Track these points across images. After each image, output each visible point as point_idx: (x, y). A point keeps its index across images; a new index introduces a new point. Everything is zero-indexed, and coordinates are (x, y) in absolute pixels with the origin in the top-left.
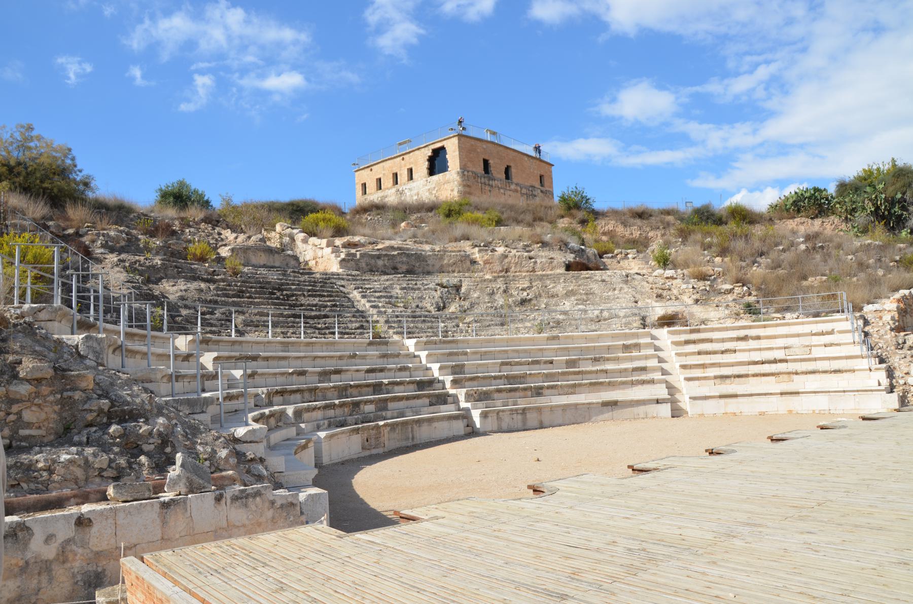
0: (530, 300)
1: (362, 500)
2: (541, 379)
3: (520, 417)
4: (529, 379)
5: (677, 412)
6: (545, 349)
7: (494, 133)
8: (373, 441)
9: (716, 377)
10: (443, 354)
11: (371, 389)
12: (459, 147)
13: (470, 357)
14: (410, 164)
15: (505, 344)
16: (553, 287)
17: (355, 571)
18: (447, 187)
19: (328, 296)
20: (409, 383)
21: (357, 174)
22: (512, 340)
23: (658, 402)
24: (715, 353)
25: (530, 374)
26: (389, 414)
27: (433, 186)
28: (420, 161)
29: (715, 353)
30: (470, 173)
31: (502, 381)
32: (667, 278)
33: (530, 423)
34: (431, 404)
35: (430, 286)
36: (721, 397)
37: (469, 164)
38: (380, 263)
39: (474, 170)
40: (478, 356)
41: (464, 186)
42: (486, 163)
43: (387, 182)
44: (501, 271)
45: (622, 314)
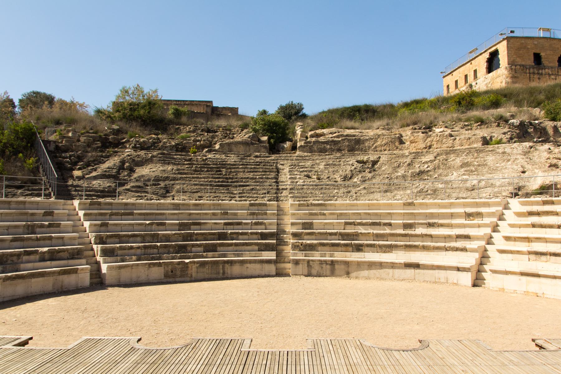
0: (428, 171)
1: (24, 303)
2: (372, 238)
3: (328, 267)
4: (361, 237)
5: (477, 282)
6: (393, 213)
7: (545, 30)
8: (178, 273)
9: (530, 253)
10: (305, 214)
12: (508, 47)
13: (269, 217)
14: (476, 66)
15: (35, 206)
16: (453, 160)
17: (302, 363)
18: (500, 79)
19: (262, 172)
22: (373, 205)
23: (458, 269)
24: (551, 227)
25: (361, 233)
27: (489, 81)
28: (481, 63)
29: (551, 227)
30: (518, 67)
31: (337, 237)
33: (314, 272)
34: (260, 250)
36: (523, 274)
39: (523, 63)
40: (336, 216)
41: (512, 77)
42: (537, 58)
43: (461, 83)
44: (426, 148)
45: (498, 184)
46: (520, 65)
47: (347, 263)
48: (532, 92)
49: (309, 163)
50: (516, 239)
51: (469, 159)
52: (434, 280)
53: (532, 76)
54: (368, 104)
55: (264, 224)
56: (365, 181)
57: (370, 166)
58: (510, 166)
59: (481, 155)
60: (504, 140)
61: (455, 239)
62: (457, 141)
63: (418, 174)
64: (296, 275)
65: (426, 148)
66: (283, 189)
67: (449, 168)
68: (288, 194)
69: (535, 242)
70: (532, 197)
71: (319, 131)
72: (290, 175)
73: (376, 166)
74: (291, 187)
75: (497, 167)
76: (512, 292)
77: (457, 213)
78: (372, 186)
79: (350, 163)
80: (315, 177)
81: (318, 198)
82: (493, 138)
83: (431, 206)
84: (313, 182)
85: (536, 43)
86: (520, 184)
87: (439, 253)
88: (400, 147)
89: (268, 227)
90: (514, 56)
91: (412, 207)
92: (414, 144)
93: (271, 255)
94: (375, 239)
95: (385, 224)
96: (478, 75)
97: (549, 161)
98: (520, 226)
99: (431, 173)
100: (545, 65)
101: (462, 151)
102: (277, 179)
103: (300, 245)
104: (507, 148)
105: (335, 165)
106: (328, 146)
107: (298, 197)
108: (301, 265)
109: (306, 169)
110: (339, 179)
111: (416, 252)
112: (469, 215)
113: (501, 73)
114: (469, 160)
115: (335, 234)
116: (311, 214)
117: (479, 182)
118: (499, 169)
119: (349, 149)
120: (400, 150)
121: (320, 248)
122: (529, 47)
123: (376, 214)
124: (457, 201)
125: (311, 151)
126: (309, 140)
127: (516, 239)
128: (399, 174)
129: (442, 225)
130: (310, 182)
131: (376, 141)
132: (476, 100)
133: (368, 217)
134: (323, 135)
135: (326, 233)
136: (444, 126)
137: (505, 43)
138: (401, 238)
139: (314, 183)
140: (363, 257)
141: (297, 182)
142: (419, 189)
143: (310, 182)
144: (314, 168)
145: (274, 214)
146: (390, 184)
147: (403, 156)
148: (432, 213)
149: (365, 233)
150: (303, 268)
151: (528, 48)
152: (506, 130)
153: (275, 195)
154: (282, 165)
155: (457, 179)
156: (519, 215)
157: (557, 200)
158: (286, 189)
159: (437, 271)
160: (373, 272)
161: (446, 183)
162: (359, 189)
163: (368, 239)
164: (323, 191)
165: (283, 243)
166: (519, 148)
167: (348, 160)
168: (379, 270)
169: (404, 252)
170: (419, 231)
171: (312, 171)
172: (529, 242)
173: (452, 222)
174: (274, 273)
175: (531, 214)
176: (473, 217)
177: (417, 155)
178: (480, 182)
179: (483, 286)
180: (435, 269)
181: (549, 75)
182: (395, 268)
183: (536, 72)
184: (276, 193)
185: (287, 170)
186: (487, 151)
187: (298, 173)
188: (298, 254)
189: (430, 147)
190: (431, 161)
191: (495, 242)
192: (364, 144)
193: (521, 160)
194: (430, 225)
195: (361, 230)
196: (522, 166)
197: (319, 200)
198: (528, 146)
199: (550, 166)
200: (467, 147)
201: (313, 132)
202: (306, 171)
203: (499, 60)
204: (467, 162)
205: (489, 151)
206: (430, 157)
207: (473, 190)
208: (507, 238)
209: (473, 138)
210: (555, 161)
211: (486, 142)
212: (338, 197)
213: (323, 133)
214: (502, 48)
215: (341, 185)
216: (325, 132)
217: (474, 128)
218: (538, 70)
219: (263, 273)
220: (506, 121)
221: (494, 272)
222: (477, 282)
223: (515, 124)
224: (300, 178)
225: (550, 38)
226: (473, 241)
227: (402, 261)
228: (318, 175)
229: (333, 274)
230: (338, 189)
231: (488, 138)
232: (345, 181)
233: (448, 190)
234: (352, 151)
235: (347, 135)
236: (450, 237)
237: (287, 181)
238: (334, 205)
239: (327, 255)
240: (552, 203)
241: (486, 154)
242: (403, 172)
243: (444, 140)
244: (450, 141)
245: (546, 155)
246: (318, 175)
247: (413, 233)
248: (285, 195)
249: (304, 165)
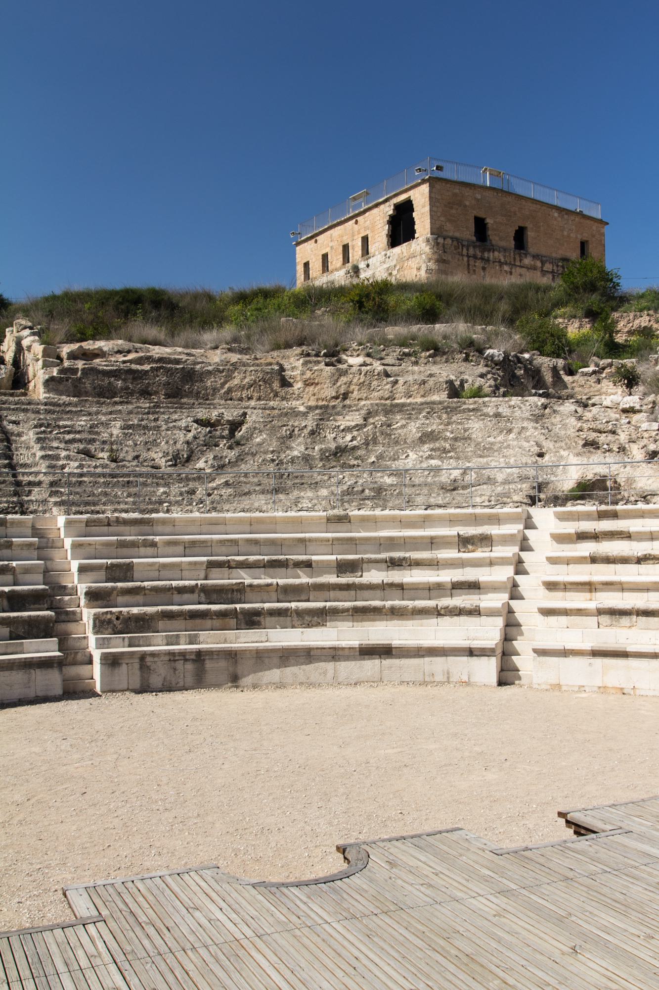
0: (354, 448)
2: (274, 596)
3: (189, 666)
4: (249, 595)
5: (507, 676)
6: (310, 540)
9: (600, 612)
10: (108, 544)
12: (430, 197)
13: (16, 552)
14: (366, 228)
15: (248, 528)
16: (403, 426)
18: (414, 262)
21: (298, 248)
22: (260, 521)
23: (471, 652)
24: (624, 560)
25: (251, 586)
27: (394, 262)
29: (624, 560)
30: (449, 241)
31: (195, 597)
32: (625, 411)
33: (155, 681)
35: (179, 424)
36: (596, 653)
37: (448, 226)
39: (457, 235)
40: (180, 549)
42: (480, 226)
43: (336, 260)
44: (336, 398)
45: (500, 477)
46: (452, 238)
47: (232, 656)
48: (488, 294)
49: (82, 422)
50: (566, 587)
51: (434, 425)
52: (421, 678)
53: (472, 263)
54: (157, 288)
55: (12, 570)
56: (222, 467)
57: (226, 432)
58: (515, 443)
59: (454, 418)
60: (487, 390)
61: (449, 592)
62: (400, 387)
63: (335, 454)
64: (113, 691)
65: (336, 398)
66: (30, 483)
67: (397, 443)
68: (45, 495)
69: (602, 590)
70: (569, 504)
71: (89, 345)
72: (42, 448)
73: (238, 435)
74: (51, 478)
75: (492, 444)
76: (576, 689)
77: (443, 537)
78: (242, 479)
79: (181, 426)
80: (105, 455)
81: (122, 506)
82: (466, 385)
83: (382, 523)
84: (104, 466)
85: (479, 196)
86: (540, 480)
87: (425, 621)
88: (282, 393)
89: (20, 577)
90: (442, 219)
91: (346, 526)
92: (311, 388)
93: (45, 648)
94: (281, 597)
95: (298, 564)
96: (371, 249)
97: (583, 435)
98: (569, 561)
99: (360, 453)
100: (494, 242)
101: (419, 408)
102: (10, 458)
103: (114, 618)
104: (493, 404)
105: (145, 427)
106: (120, 383)
107: (73, 504)
108: (124, 667)
109: (78, 436)
110: (162, 462)
111: (378, 623)
112: (465, 542)
113: (418, 249)
114: (434, 427)
115: (191, 590)
116: (122, 545)
117: (464, 473)
118: (495, 448)
119: (169, 391)
120: (283, 399)
121: (161, 624)
122: (467, 203)
123: (272, 542)
124: (429, 512)
125: (77, 392)
126: (66, 364)
127: (566, 587)
128: (296, 453)
129: (418, 564)
130: (96, 467)
131: (229, 377)
132: (391, 300)
133: (254, 549)
134: (99, 354)
135: (170, 589)
136: (364, 352)
137: (425, 188)
138: (339, 594)
139: (107, 471)
140: (264, 639)
141: (63, 467)
142: (345, 487)
143: (96, 467)
144: (98, 433)
145: (30, 545)
146: (282, 476)
147: (295, 413)
148: (391, 539)
149: (259, 586)
150: (128, 673)
151: (465, 206)
152: (482, 369)
153: (15, 499)
154: (14, 422)
155: (418, 466)
156: (560, 539)
157: (624, 510)
158: (39, 483)
159: (427, 660)
160: (290, 671)
161: (397, 473)
162: (213, 485)
163: (265, 598)
164: (133, 490)
165: (63, 617)
166: (524, 408)
167: (176, 417)
168: (304, 667)
169: (351, 624)
170: (374, 576)
171: (94, 440)
172: (591, 591)
173: (439, 556)
174: (59, 691)
175: (582, 537)
176: (473, 544)
177: (326, 412)
178: (465, 472)
179: (517, 682)
180: (423, 656)
181: (501, 264)
182: (339, 660)
183: (479, 254)
184: (16, 494)
185: (30, 436)
186: (464, 411)
187: (62, 445)
188: (113, 642)
189: (345, 396)
190: (359, 427)
191: (524, 594)
192: (202, 381)
193: (533, 432)
194: (395, 564)
195: (246, 578)
196: (538, 445)
197: (126, 511)
198: (540, 404)
199: (584, 445)
200: (419, 400)
201: (74, 346)
202: (80, 441)
203: (413, 223)
204: (433, 432)
205: (470, 410)
206: (353, 419)
207: (454, 490)
208: (551, 586)
209: (431, 382)
210: (592, 436)
211: (455, 391)
212: (170, 502)
213: (100, 349)
214: (420, 197)
215: (170, 475)
216: (105, 349)
217: (422, 360)
218: (483, 252)
219: (32, 694)
220: (481, 351)
221: (541, 653)
222: (507, 676)
223: (496, 358)
224: (68, 458)
225: (502, 191)
226: (486, 593)
227: (355, 643)
228: (112, 450)
229: (200, 682)
230: (167, 485)
231: (457, 383)
232: (175, 465)
233: (407, 490)
234: (174, 397)
235: (161, 360)
236: (439, 586)
237: (36, 464)
238: (173, 522)
239: (182, 640)
240: (615, 515)
241: (465, 415)
242: (302, 448)
243: (375, 383)
244: (386, 386)
245: (572, 421)
246: (112, 450)
247: (357, 580)
248: (40, 498)
249: (72, 426)
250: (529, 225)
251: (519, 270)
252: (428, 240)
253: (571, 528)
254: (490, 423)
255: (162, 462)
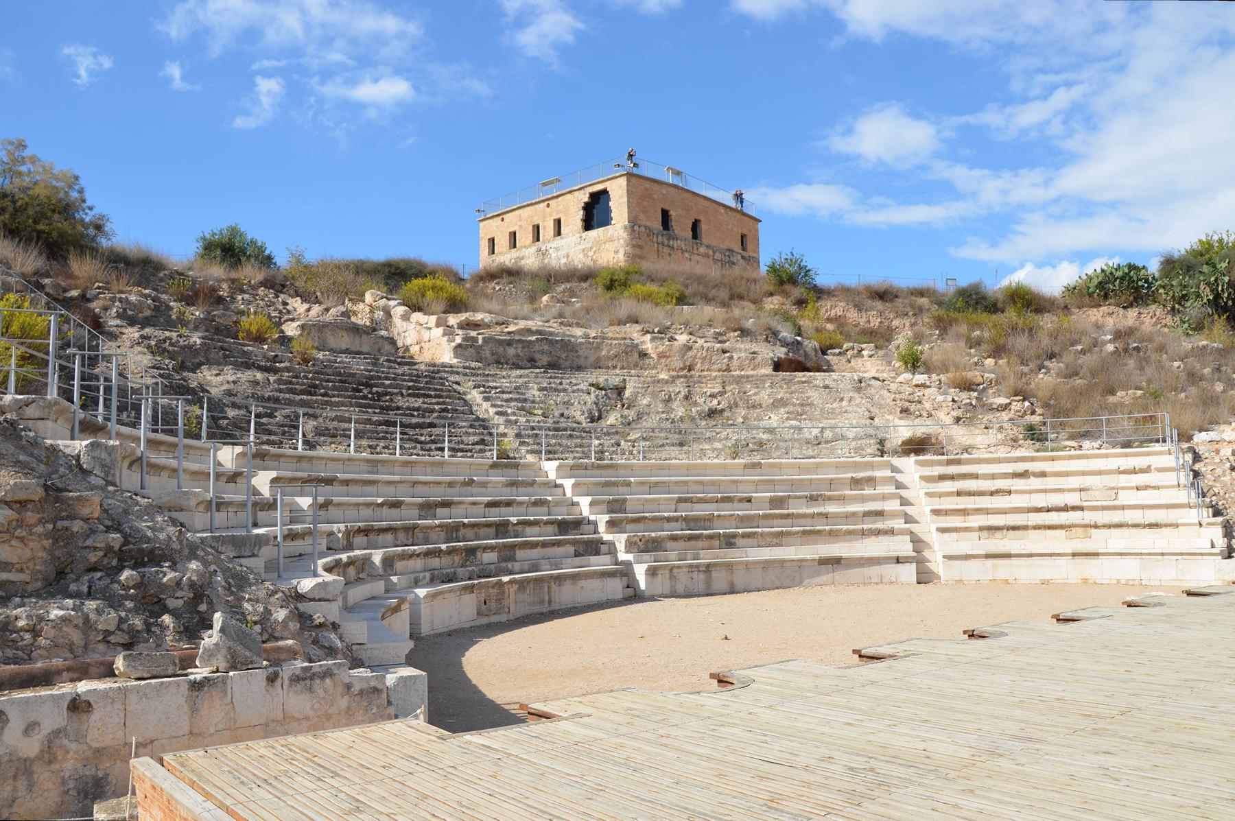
0: (722, 411)
1: (475, 687)
2: (734, 523)
3: (702, 576)
4: (716, 523)
5: (925, 577)
6: (741, 482)
7: (678, 173)
9: (981, 529)
11: (492, 530)
15: (685, 472)
16: (755, 394)
18: (610, 247)
19: (436, 397)
20: (547, 523)
21: (482, 224)
22: (695, 466)
23: (898, 560)
24: (981, 494)
25: (719, 516)
26: (517, 566)
28: (572, 208)
29: (981, 494)
30: (643, 229)
31: (678, 525)
37: (641, 216)
38: (511, 351)
39: (648, 224)
40: (646, 488)
43: (525, 238)
45: (851, 434)
91: (757, 471)
110: (582, 419)
133: (700, 488)
137: (623, 182)
175: (942, 478)
181: (683, 252)
204: (782, 399)
250: (702, 218)
251: (696, 258)
252: (626, 228)
253: (937, 471)
254: (824, 393)
255: (582, 419)
